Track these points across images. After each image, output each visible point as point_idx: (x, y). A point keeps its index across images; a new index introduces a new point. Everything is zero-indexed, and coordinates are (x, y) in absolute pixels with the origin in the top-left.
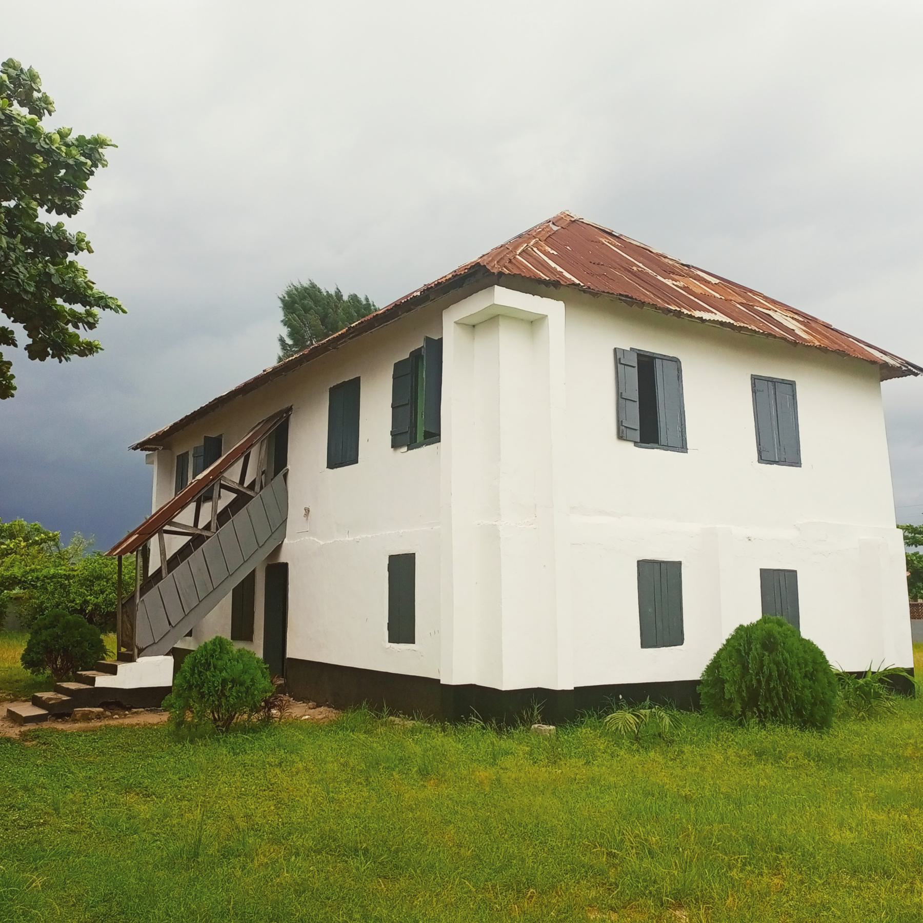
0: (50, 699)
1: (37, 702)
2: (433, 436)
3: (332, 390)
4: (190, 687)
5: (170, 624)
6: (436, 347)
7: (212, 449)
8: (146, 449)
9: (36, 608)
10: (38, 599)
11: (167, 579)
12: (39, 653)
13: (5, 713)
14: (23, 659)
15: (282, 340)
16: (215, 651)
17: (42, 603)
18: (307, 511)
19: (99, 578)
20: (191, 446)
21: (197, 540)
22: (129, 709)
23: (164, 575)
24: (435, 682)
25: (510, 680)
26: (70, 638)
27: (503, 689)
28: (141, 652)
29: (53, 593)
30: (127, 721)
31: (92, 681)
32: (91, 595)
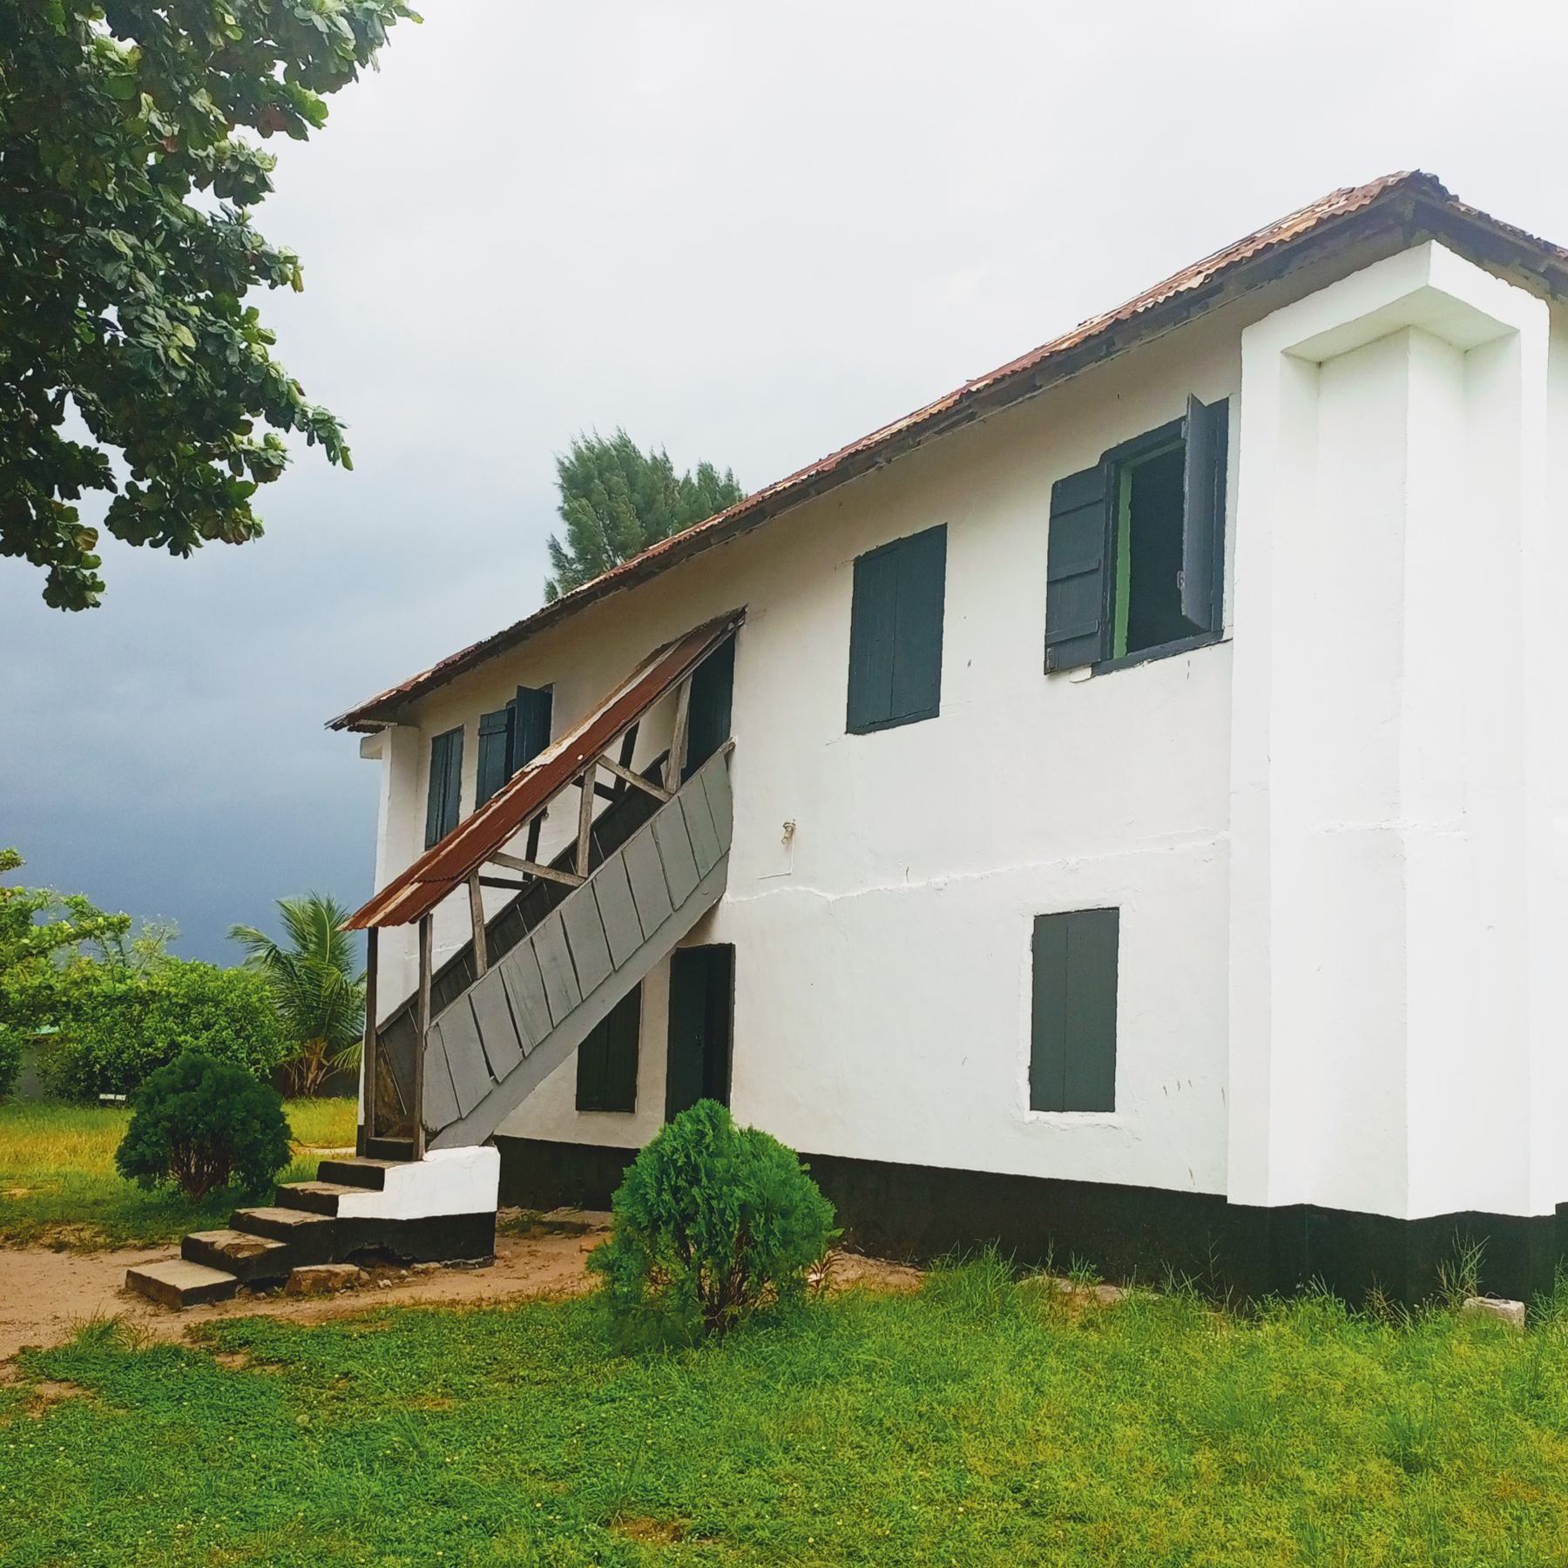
0: (239, 1248)
1: (196, 1253)
2: (1206, 628)
3: (858, 562)
4: (655, 1225)
5: (491, 1073)
6: (1215, 423)
7: (529, 720)
8: (359, 729)
9: (77, 1060)
10: (81, 1041)
11: (486, 987)
12: (157, 1144)
13: (122, 1279)
14: (121, 1156)
15: (555, 548)
16: (702, 1134)
17: (89, 1050)
18: (790, 829)
19: (200, 1000)
20: (467, 719)
21: (537, 899)
22: (407, 1265)
23: (480, 970)
24: (1217, 1202)
25: (1419, 1198)
26: (215, 1111)
27: (1412, 1214)
28: (432, 1136)
29: (110, 1031)
30: (402, 1295)
31: (331, 1204)
32: (185, 1032)
